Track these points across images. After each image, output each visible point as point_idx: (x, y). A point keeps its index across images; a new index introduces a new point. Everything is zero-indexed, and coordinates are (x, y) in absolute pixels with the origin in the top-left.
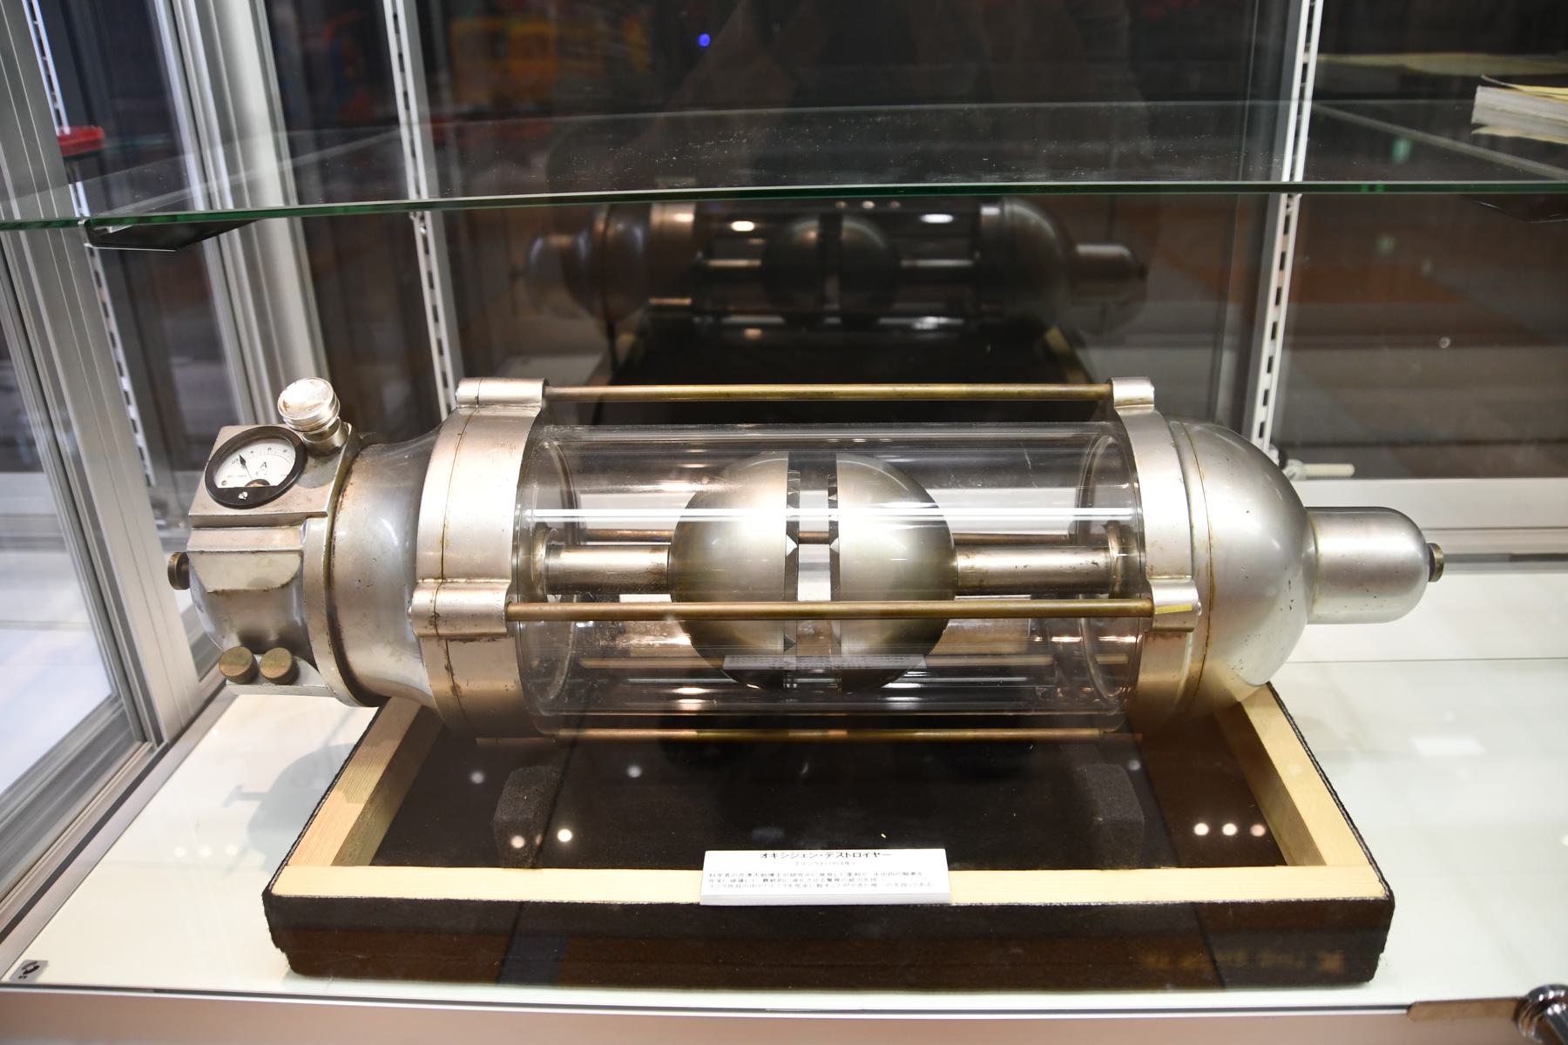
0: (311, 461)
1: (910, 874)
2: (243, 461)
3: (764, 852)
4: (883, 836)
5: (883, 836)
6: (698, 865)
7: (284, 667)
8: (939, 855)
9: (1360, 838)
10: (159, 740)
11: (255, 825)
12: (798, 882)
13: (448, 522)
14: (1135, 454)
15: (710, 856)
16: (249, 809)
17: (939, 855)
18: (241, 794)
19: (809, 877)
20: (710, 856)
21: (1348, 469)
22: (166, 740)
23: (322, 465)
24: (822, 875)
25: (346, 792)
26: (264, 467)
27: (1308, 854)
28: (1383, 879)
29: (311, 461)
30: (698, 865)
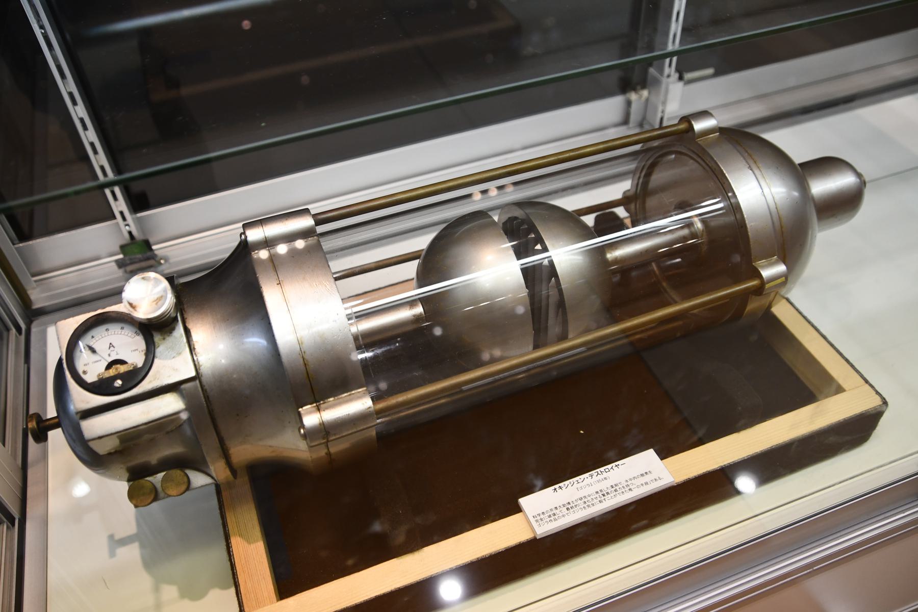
0: (157, 338)
1: (645, 474)
2: (93, 351)
3: (553, 488)
4: (582, 432)
5: (582, 432)
6: (518, 509)
7: (184, 483)
8: (651, 454)
9: (852, 366)
10: (11, 520)
11: (149, 564)
12: (588, 504)
13: (307, 361)
14: (730, 181)
15: (524, 501)
16: (132, 553)
17: (651, 454)
18: (116, 543)
19: (591, 497)
20: (524, 501)
21: (710, 71)
22: (17, 516)
23: (169, 336)
24: (597, 492)
25: (241, 536)
26: (112, 348)
27: (832, 387)
28: (877, 393)
29: (157, 338)
30: (518, 509)
